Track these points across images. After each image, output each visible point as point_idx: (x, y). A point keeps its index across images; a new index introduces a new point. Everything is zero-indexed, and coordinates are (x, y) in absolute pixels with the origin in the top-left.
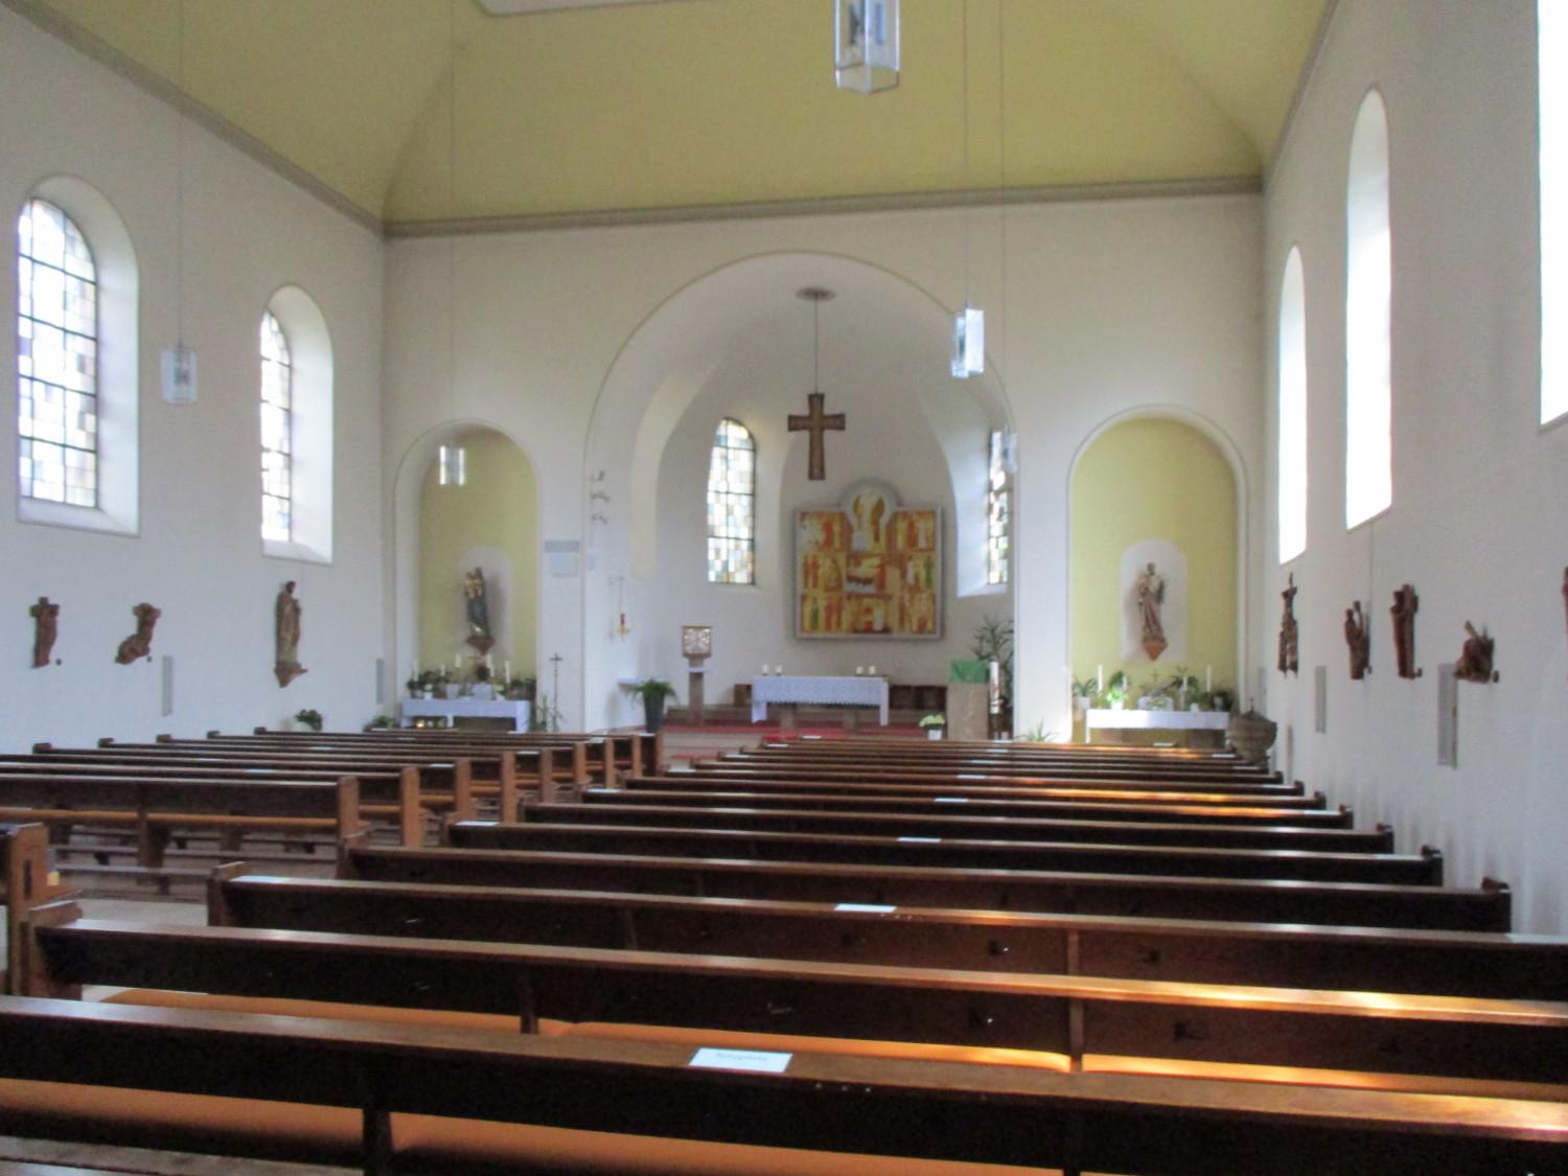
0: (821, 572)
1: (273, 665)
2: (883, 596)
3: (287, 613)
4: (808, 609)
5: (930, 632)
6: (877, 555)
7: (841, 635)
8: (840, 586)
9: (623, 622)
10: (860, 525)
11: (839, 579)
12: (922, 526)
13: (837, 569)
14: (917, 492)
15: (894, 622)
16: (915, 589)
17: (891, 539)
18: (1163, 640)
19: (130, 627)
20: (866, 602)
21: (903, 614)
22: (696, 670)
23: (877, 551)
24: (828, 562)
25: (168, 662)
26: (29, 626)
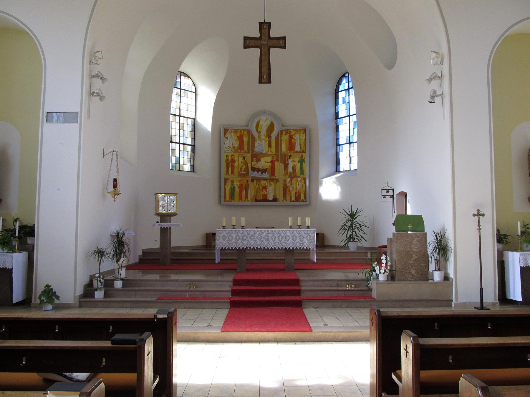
0: (236, 164)
4: (228, 188)
5: (303, 201)
8: (248, 174)
10: (259, 137)
11: (247, 169)
12: (298, 139)
13: (246, 164)
15: (280, 196)
16: (293, 175)
20: (263, 182)
22: (164, 225)
23: (269, 153)
24: (241, 159)
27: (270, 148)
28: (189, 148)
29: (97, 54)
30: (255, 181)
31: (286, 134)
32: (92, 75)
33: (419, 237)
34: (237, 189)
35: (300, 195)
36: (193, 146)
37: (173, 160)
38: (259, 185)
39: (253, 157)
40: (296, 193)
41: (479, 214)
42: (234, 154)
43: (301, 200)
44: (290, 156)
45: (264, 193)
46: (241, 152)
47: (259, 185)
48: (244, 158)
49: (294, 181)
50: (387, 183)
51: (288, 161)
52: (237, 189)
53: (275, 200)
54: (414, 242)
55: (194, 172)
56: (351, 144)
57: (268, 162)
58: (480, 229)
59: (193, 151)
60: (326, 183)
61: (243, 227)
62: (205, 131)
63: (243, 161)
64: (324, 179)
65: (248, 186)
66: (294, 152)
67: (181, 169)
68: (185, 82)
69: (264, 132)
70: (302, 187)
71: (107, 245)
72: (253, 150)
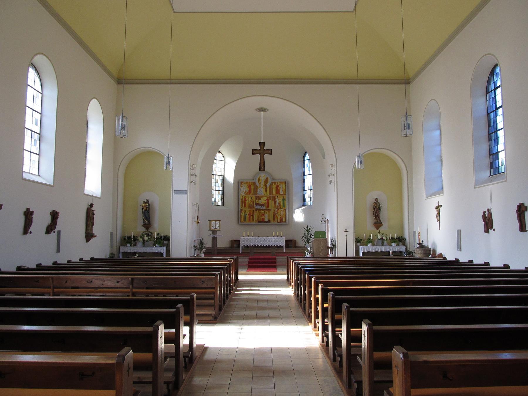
0: (247, 202)
4: (243, 215)
5: (284, 222)
7: (254, 223)
10: (260, 186)
12: (282, 187)
13: (252, 201)
15: (271, 219)
16: (279, 207)
17: (270, 192)
18: (381, 223)
20: (262, 211)
21: (274, 215)
22: (214, 235)
23: (266, 195)
24: (250, 199)
25: (59, 232)
28: (221, 192)
30: (258, 211)
31: (275, 184)
33: (323, 240)
34: (247, 216)
36: (223, 191)
37: (213, 200)
39: (256, 197)
40: (281, 217)
41: (346, 231)
42: (246, 196)
44: (277, 197)
45: (262, 218)
47: (260, 213)
48: (251, 198)
49: (280, 210)
50: (323, 215)
51: (276, 199)
52: (247, 216)
53: (269, 221)
54: (322, 242)
56: (311, 191)
57: (265, 200)
58: (346, 237)
59: (223, 194)
60: (297, 212)
61: (252, 236)
62: (229, 183)
64: (296, 210)
65: (254, 213)
66: (280, 195)
67: (217, 205)
69: (262, 183)
70: (284, 214)
72: (256, 193)
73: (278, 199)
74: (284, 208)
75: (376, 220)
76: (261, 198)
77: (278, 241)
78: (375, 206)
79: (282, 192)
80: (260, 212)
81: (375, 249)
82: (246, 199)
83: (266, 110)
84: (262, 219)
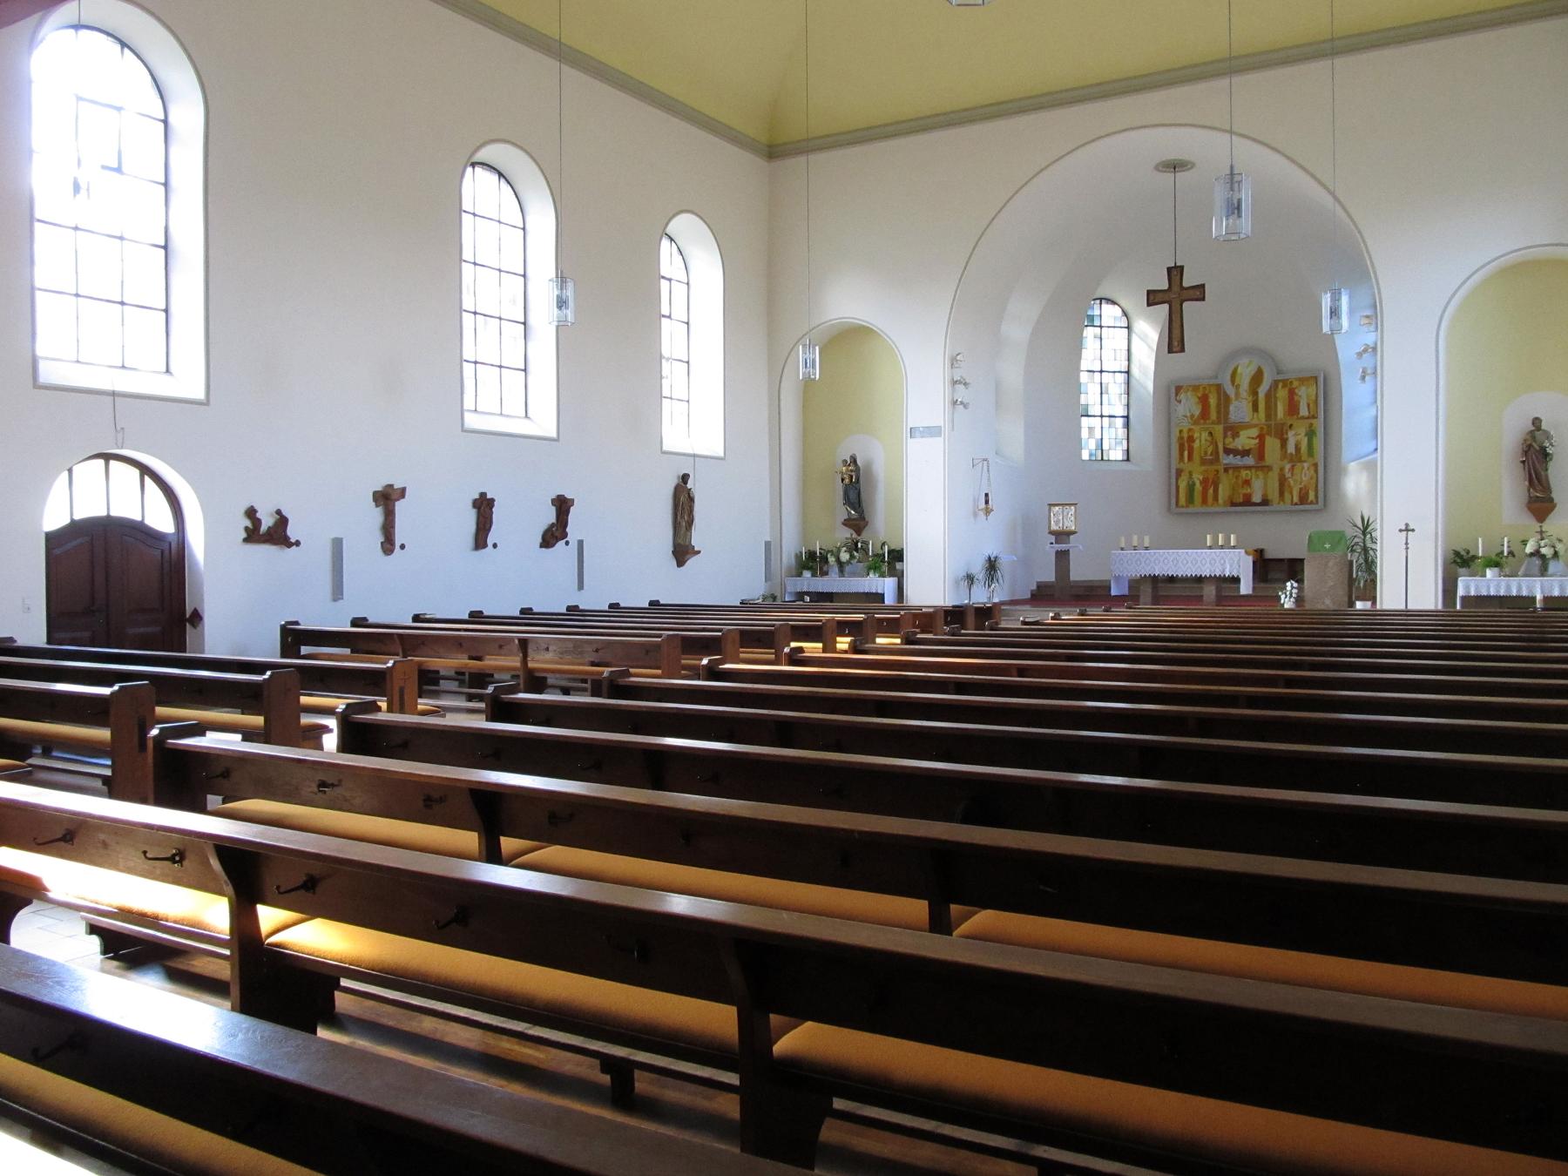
0: (1196, 445)
1: (670, 548)
2: (1262, 467)
3: (683, 503)
4: (1183, 485)
5: (1312, 503)
6: (1255, 426)
8: (1216, 459)
9: (987, 502)
10: (1237, 395)
11: (1216, 452)
12: (1304, 394)
14: (1296, 358)
15: (1273, 494)
16: (1296, 459)
18: (1551, 500)
19: (550, 516)
20: (1244, 473)
21: (1283, 482)
22: (1063, 547)
23: (1255, 421)
24: (1205, 435)
26: (470, 517)
27: (1255, 414)
28: (1120, 422)
29: (958, 358)
30: (1231, 472)
32: (955, 379)
34: (1198, 487)
35: (1307, 493)
36: (1127, 417)
37: (1092, 445)
38: (1237, 477)
39: (1226, 430)
40: (1301, 489)
41: (1407, 529)
43: (1309, 501)
44: (1291, 426)
45: (1245, 491)
46: (1205, 423)
47: (1237, 477)
48: (1211, 434)
49: (1297, 471)
51: (1287, 434)
52: (1198, 487)
53: (1265, 502)
54: (1331, 564)
55: (1128, 460)
57: (1253, 438)
58: (1407, 548)
59: (1127, 425)
61: (1147, 548)
63: (1209, 439)
66: (1298, 419)
67: (1105, 458)
68: (1110, 313)
69: (1245, 382)
70: (1311, 478)
71: (978, 569)
73: (1293, 432)
74: (1310, 459)
75: (1531, 490)
76: (1241, 433)
77: (1178, 561)
78: (1529, 442)
79: (1306, 409)
80: (1236, 474)
81: (1508, 587)
82: (1192, 436)
83: (1186, 165)
84: (1245, 495)
